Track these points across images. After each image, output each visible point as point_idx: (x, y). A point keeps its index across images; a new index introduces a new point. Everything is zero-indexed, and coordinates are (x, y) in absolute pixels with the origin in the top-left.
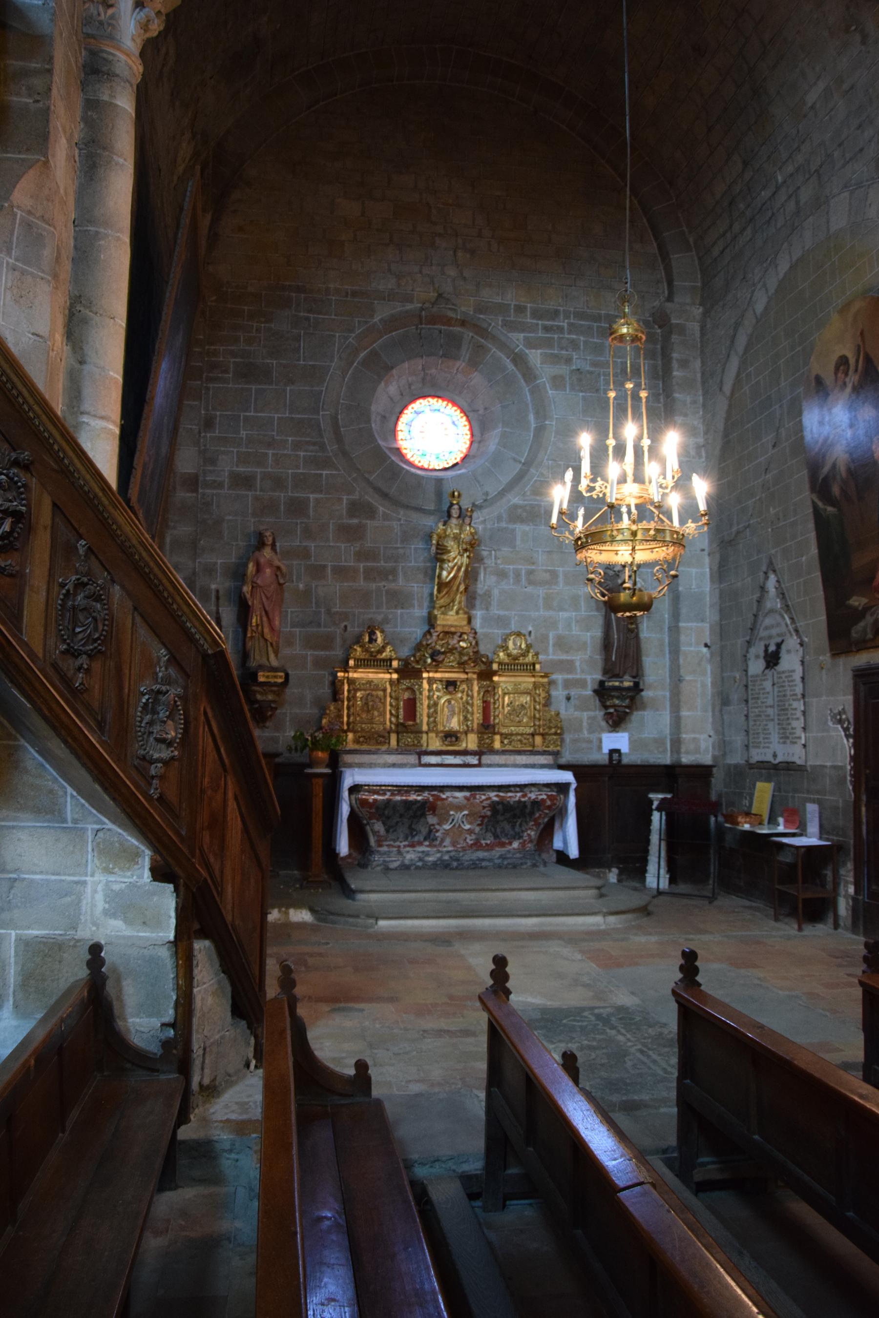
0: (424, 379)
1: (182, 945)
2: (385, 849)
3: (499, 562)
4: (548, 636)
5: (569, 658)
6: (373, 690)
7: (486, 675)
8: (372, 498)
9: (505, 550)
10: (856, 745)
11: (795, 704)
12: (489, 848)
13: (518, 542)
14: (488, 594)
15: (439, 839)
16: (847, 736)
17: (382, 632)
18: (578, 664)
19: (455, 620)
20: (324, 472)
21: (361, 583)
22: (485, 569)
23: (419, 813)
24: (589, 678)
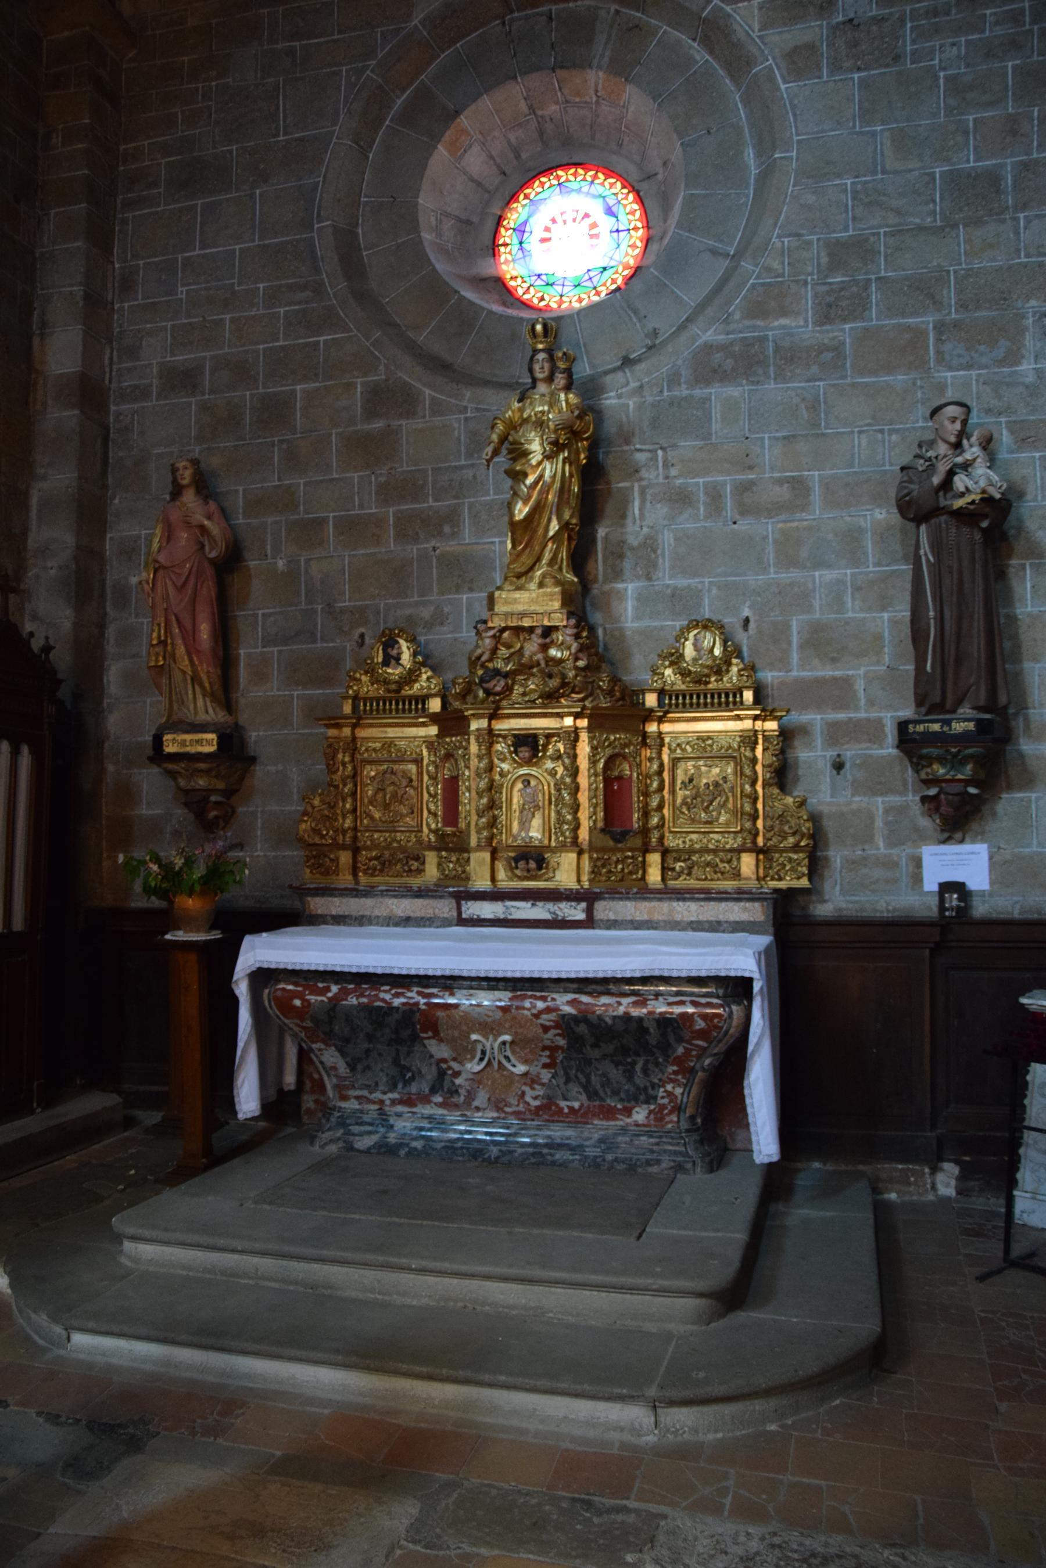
0: (541, 133)
2: (352, 1105)
3: (673, 472)
4: (787, 627)
5: (838, 673)
6: (394, 762)
9: (688, 445)
12: (578, 1117)
13: (715, 426)
14: (650, 545)
15: (462, 1092)
17: (412, 640)
18: (860, 685)
19: (532, 601)
20: (321, 339)
21: (391, 546)
22: (643, 492)
23: (405, 1034)
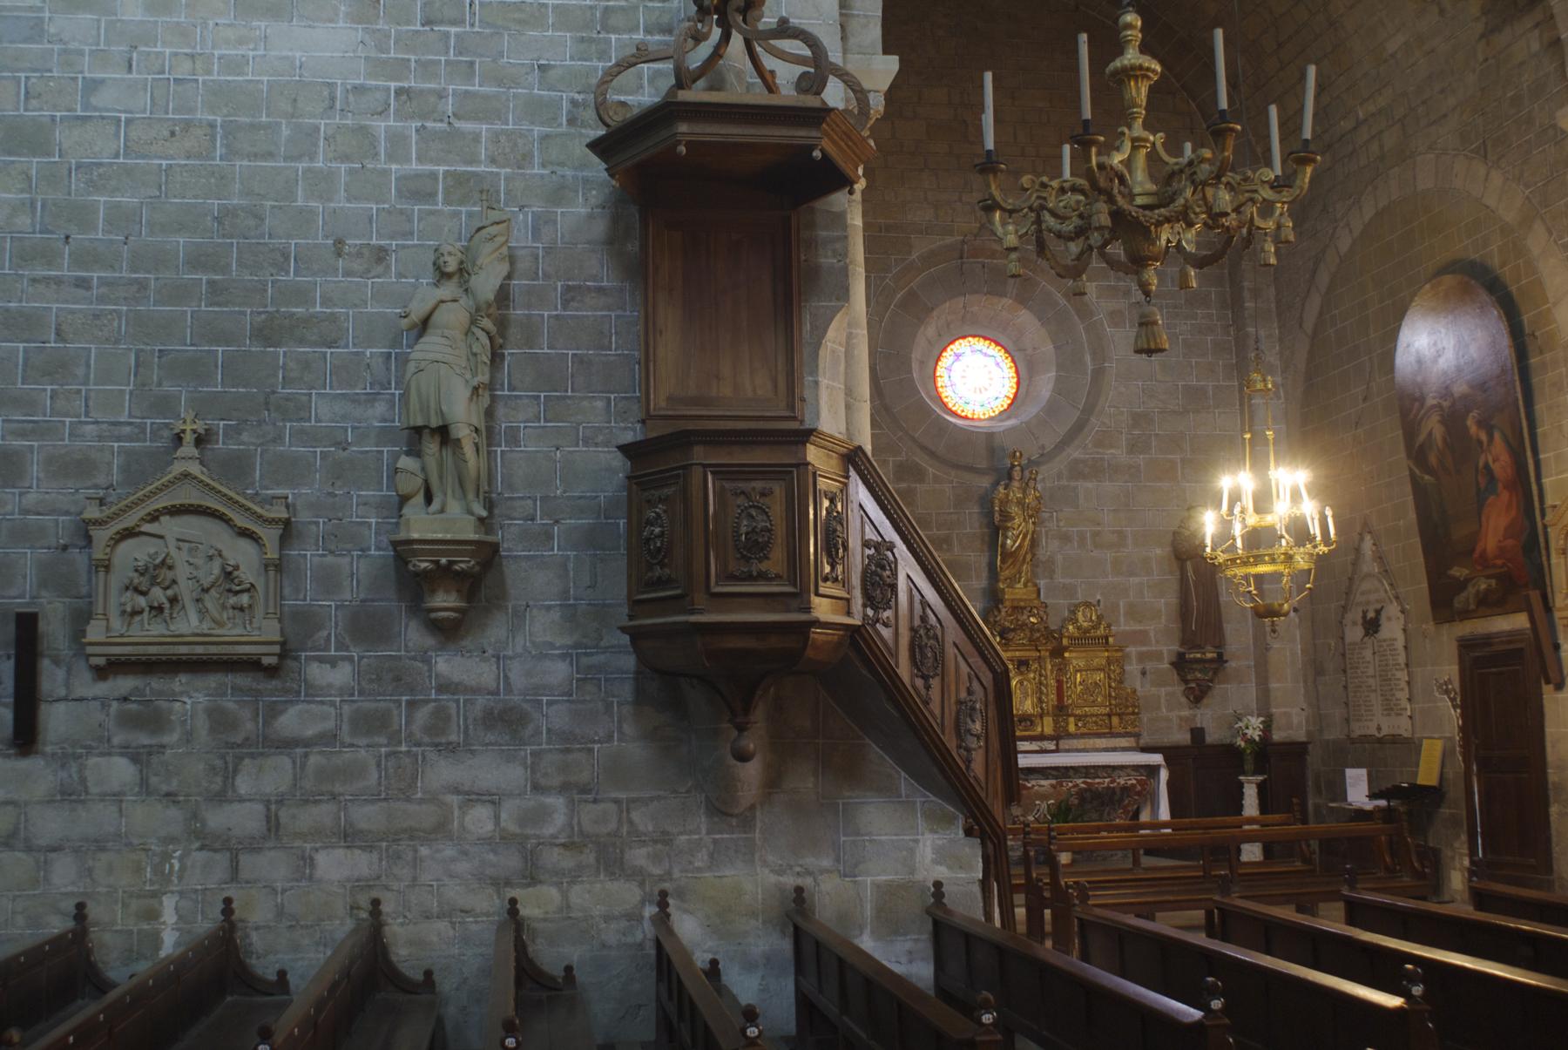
1: (985, 884)
7: (1058, 652)
8: (921, 460)
10: (1463, 715)
11: (1399, 674)
16: (1455, 707)
24: (1165, 649)
